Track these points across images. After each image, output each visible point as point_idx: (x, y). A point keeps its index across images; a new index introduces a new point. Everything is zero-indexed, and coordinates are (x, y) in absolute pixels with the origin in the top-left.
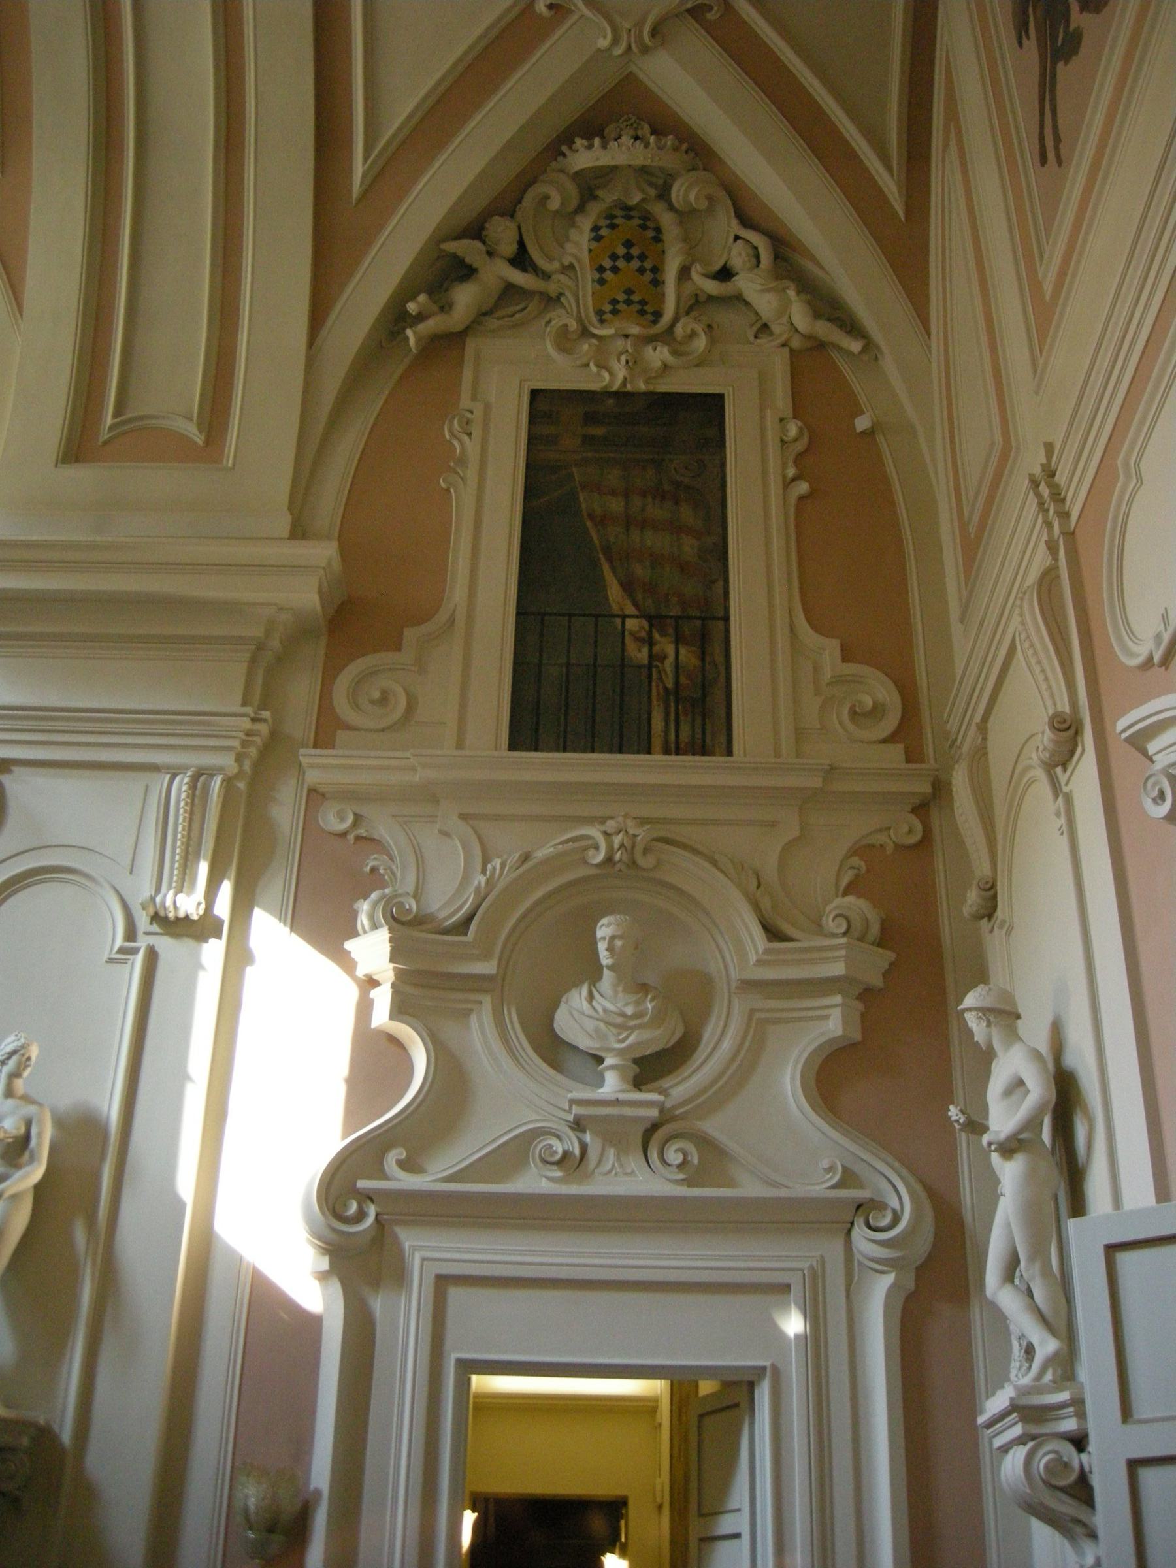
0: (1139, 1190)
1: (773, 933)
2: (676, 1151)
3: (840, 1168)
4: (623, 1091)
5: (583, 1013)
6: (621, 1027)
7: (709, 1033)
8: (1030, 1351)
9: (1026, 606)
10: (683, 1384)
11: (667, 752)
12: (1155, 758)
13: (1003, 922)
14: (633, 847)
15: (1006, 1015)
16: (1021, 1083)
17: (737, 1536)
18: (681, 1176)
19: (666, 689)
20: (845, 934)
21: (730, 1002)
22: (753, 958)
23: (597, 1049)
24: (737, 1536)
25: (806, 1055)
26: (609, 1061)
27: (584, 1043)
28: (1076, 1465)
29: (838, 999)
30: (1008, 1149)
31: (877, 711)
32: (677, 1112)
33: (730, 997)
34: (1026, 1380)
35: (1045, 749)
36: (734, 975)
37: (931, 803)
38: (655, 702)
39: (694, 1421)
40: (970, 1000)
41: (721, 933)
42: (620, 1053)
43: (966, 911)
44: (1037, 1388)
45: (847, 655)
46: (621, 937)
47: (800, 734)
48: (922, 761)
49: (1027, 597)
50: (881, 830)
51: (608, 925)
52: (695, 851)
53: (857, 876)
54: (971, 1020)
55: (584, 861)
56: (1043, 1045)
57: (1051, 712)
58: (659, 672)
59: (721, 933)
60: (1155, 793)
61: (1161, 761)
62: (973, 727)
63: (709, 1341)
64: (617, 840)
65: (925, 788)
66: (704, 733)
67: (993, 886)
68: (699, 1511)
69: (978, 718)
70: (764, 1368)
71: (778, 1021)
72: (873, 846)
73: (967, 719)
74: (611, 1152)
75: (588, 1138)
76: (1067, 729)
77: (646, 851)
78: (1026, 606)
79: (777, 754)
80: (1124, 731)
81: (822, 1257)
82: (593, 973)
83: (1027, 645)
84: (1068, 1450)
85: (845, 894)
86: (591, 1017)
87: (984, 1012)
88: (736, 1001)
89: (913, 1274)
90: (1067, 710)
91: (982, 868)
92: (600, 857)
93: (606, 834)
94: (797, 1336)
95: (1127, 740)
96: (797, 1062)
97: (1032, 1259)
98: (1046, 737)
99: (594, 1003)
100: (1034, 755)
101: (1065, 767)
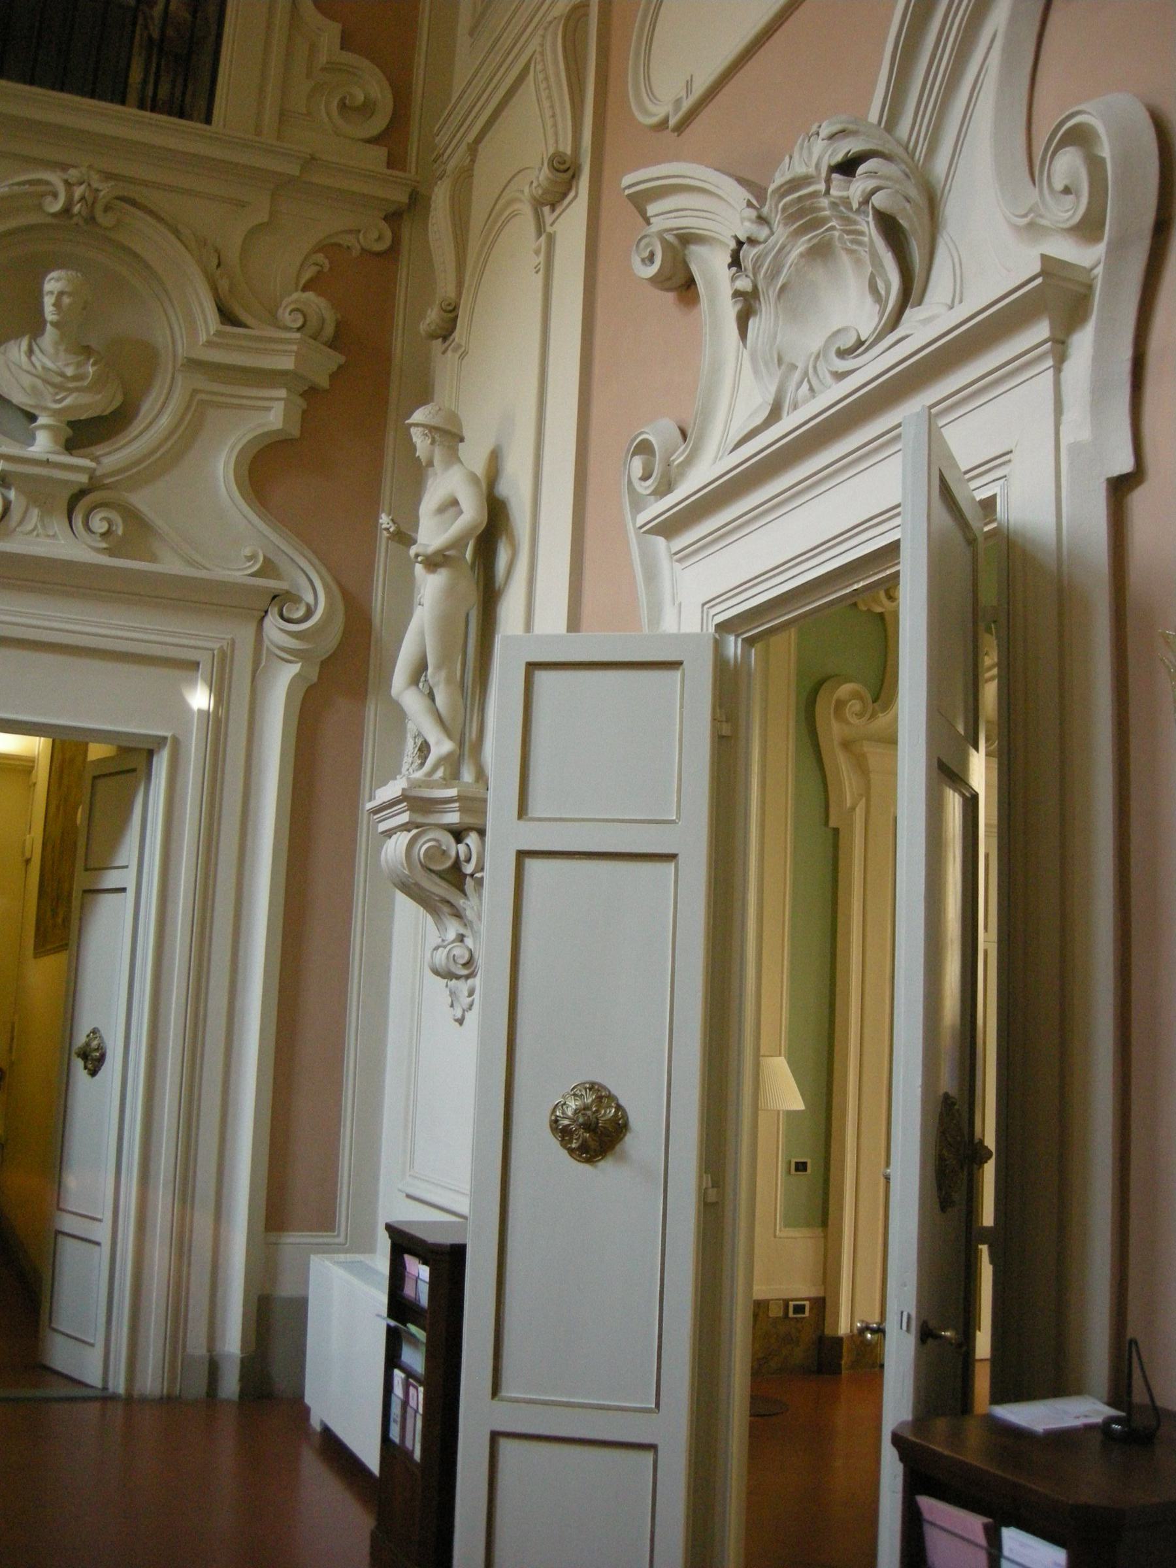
0: (552, 617)
1: (227, 316)
2: (101, 520)
3: (261, 559)
4: (54, 453)
5: (20, 367)
6: (59, 387)
7: (147, 408)
8: (424, 749)
9: (549, 38)
10: (68, 747)
11: (142, 106)
12: (652, 220)
13: (459, 346)
14: (94, 203)
15: (450, 436)
16: (455, 503)
17: (123, 890)
18: (104, 545)
19: (150, 38)
20: (299, 329)
21: (173, 378)
22: (203, 338)
23: (31, 406)
24: (123, 890)
25: (244, 441)
26: (42, 420)
27: (19, 398)
28: (453, 854)
29: (282, 393)
30: (433, 562)
31: (367, 109)
32: (107, 481)
33: (173, 374)
34: (419, 775)
35: (539, 185)
36: (180, 351)
37: (406, 213)
38: (136, 50)
39: (88, 781)
40: (419, 416)
41: (173, 306)
42: (55, 413)
43: (423, 328)
44: (427, 783)
45: (346, 43)
46: (70, 294)
47: (283, 116)
48: (404, 169)
49: (551, 30)
50: (350, 232)
51: (58, 280)
52: (160, 219)
53: (319, 272)
54: (417, 436)
55: (40, 207)
56: (479, 468)
57: (551, 151)
58: (145, 19)
59: (173, 306)
60: (646, 254)
61: (658, 224)
62: (464, 146)
63: (107, 707)
64: (78, 192)
65: (401, 197)
66: (184, 94)
67: (455, 309)
68: (86, 865)
69: (471, 138)
70: (165, 738)
71: (219, 406)
72: (340, 245)
73: (459, 135)
74: (35, 513)
75: (12, 494)
76: (565, 172)
77: (107, 208)
78: (549, 38)
79: (258, 133)
80: (630, 186)
81: (233, 641)
82: (36, 327)
83: (541, 76)
84: (448, 840)
85: (305, 289)
86: (28, 372)
87: (431, 429)
88: (179, 378)
89: (317, 669)
90: (569, 152)
91: (446, 287)
92: (57, 206)
93: (67, 183)
94: (200, 711)
95: (628, 196)
96: (232, 449)
97: (439, 667)
98: (544, 174)
99: (33, 358)
100: (526, 190)
101: (553, 208)
